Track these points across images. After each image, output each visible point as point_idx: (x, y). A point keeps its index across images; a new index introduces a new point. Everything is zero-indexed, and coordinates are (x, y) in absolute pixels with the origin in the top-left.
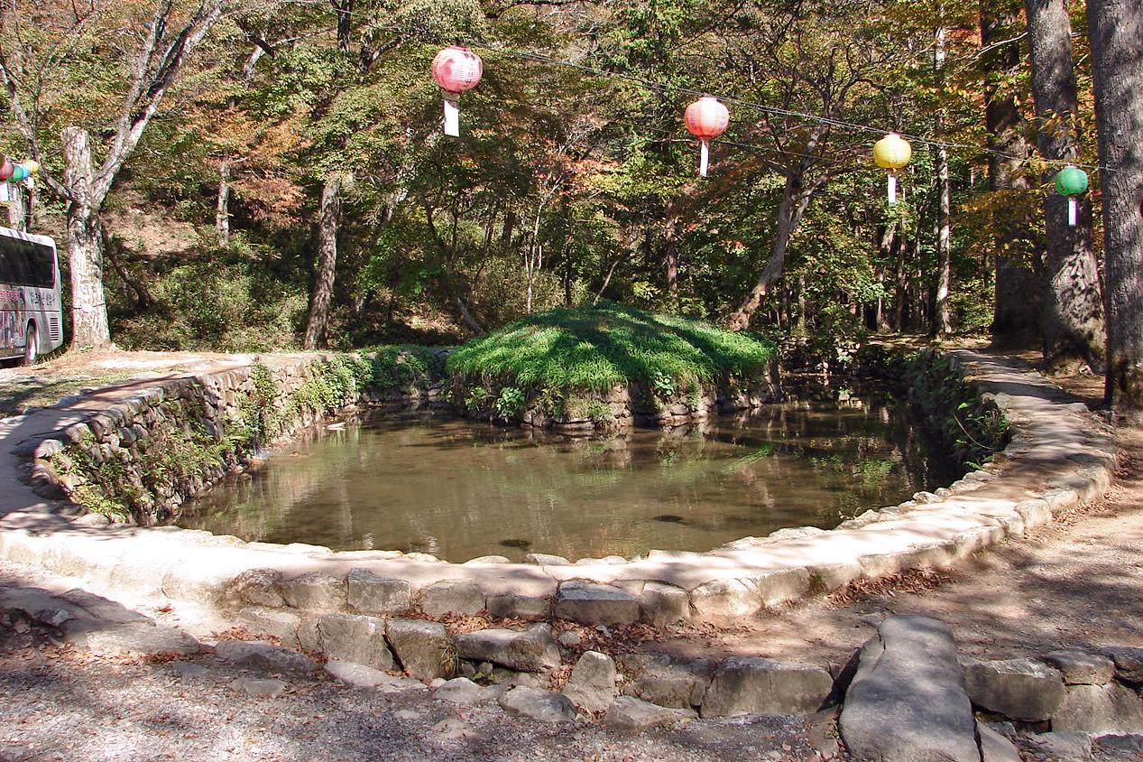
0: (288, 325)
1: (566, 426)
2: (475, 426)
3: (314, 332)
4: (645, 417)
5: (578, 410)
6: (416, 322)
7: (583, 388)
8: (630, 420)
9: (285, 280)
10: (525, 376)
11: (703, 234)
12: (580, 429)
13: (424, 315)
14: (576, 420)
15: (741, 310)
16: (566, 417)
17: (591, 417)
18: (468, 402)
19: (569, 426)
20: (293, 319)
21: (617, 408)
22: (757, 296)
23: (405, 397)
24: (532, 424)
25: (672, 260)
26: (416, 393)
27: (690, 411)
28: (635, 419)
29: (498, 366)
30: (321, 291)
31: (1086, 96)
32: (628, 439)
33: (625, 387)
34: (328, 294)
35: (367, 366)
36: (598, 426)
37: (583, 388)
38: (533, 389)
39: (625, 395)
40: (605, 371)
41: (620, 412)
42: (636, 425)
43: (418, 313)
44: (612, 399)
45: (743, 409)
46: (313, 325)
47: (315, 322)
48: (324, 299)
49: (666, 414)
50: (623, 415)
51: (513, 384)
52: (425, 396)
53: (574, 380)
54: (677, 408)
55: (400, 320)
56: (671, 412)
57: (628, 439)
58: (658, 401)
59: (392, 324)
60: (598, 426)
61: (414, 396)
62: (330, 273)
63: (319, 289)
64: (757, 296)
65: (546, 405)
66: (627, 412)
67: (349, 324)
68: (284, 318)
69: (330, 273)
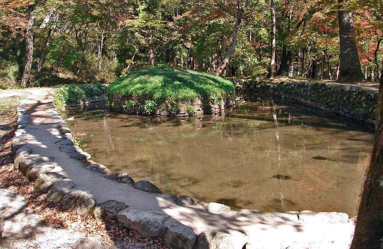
0: (13, 78)
1: (178, 115)
2: (343, 141)
3: (25, 80)
4: (207, 111)
5: (183, 108)
6: (61, 75)
7: (184, 100)
8: (202, 111)
9: (7, 59)
10: (157, 95)
11: (178, 41)
12: (184, 116)
13: (63, 72)
14: (182, 112)
15: (219, 68)
16: (178, 112)
17: (188, 111)
18: (124, 106)
19: (179, 115)
20: (15, 75)
21: (197, 108)
22: (225, 63)
23: (78, 105)
24: (160, 115)
25: (152, 51)
26: (82, 103)
27: (220, 106)
28: (204, 111)
29: (141, 92)
30: (28, 64)
31: (78, 35)
32: (201, 119)
33: (199, 99)
34: (31, 65)
35: (67, 93)
36: (191, 115)
37: (184, 100)
38: (162, 100)
39: (199, 102)
40: (191, 93)
41: (198, 109)
42: (204, 113)
43: (61, 72)
44: (195, 104)
45: (232, 106)
46: (24, 77)
47: (26, 76)
48: (29, 67)
49: (213, 109)
50: (199, 110)
51: (151, 98)
52: (84, 104)
53: (180, 97)
54: (216, 106)
55: (55, 75)
56: (215, 108)
57: (201, 119)
58: (211, 104)
59: (53, 77)
60: (191, 115)
61: (81, 104)
62: (31, 56)
63: (27, 63)
64: (225, 63)
65: (167, 107)
66: (201, 109)
67: (37, 76)
68: (11, 74)
69: (31, 56)
